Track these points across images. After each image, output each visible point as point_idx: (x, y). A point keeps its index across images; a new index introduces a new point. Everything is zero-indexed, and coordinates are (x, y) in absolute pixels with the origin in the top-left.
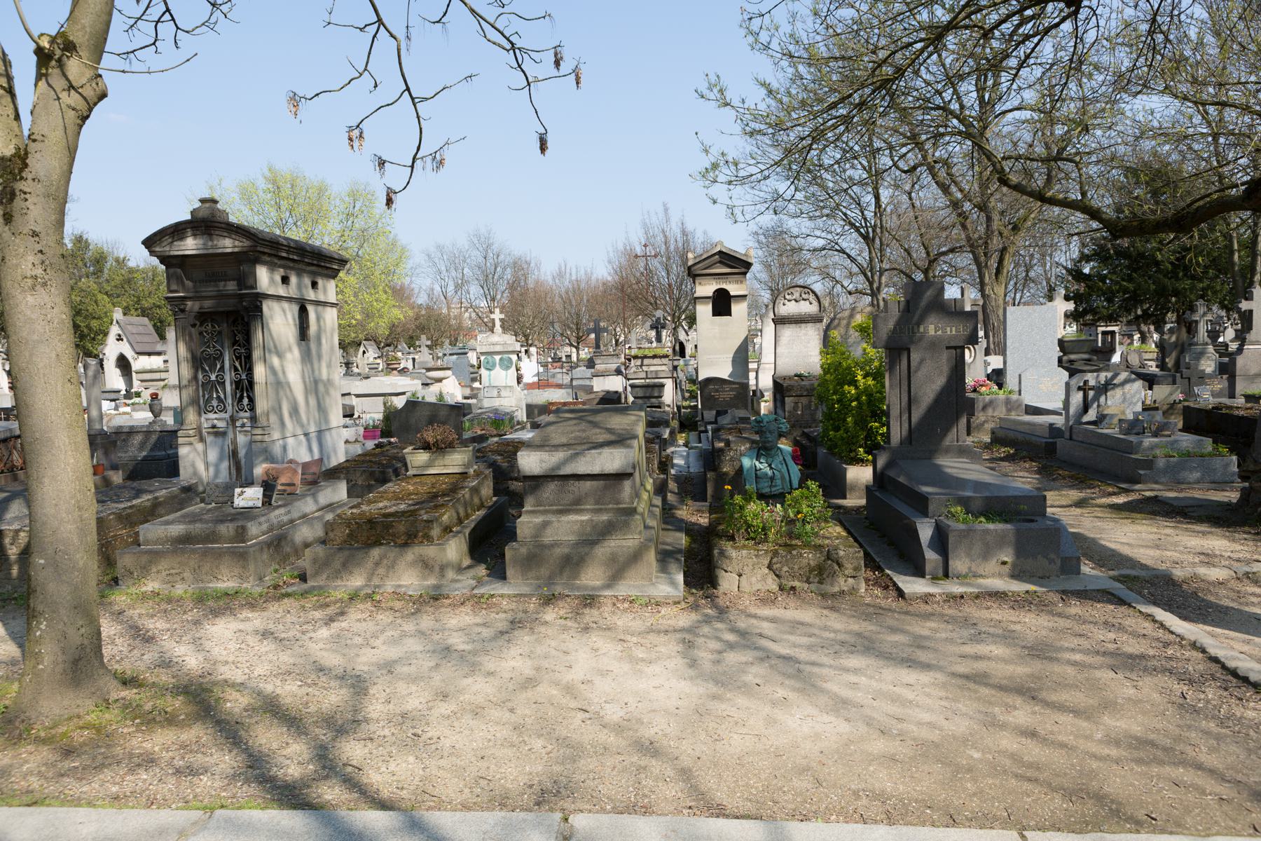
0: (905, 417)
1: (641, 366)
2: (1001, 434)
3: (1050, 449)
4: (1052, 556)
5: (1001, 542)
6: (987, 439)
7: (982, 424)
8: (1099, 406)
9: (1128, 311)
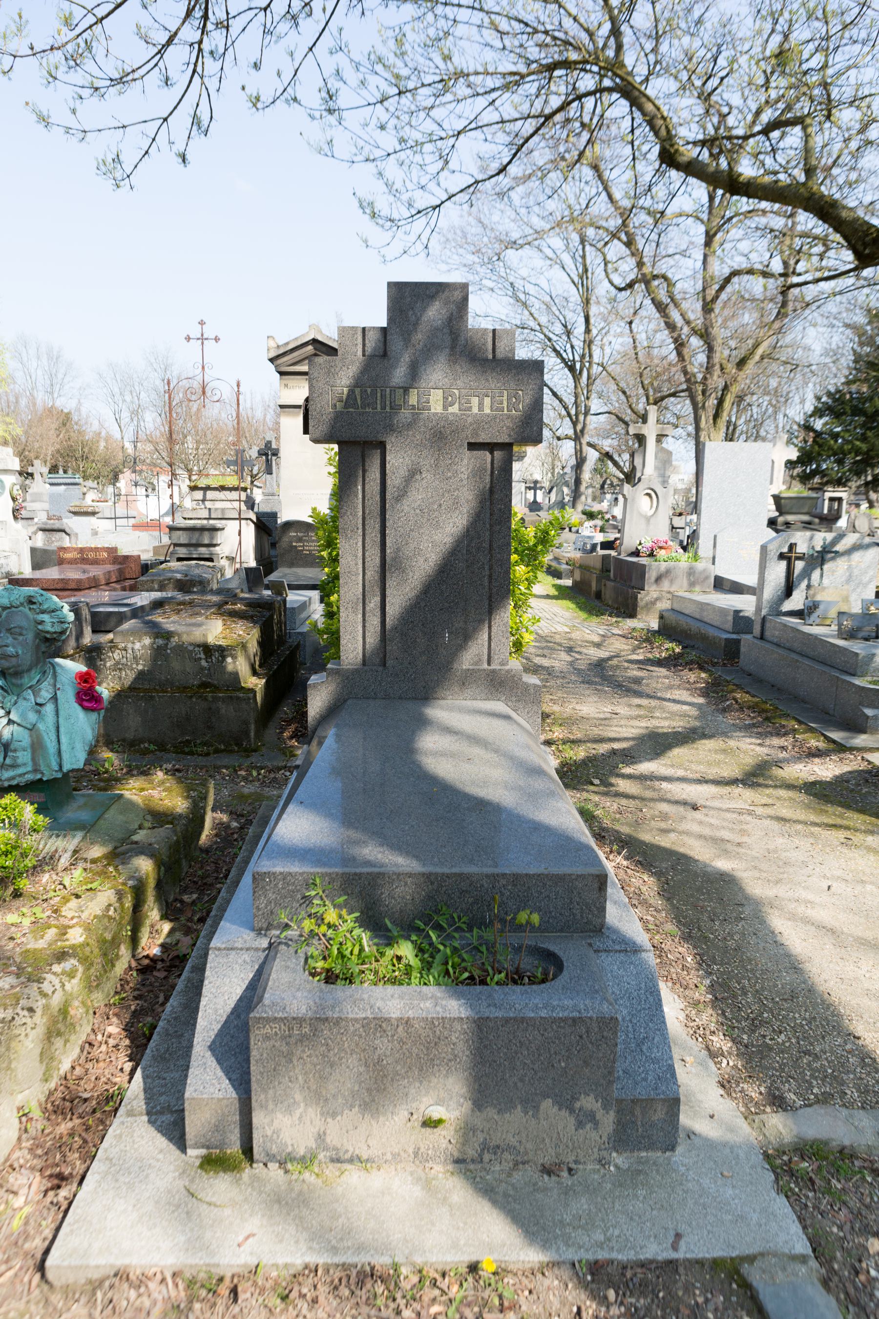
0: (374, 603)
1: (204, 500)
2: (672, 618)
3: (732, 650)
4: (588, 1102)
5: (421, 1051)
6: (655, 625)
7: (653, 603)
8: (809, 587)
9: (858, 474)
